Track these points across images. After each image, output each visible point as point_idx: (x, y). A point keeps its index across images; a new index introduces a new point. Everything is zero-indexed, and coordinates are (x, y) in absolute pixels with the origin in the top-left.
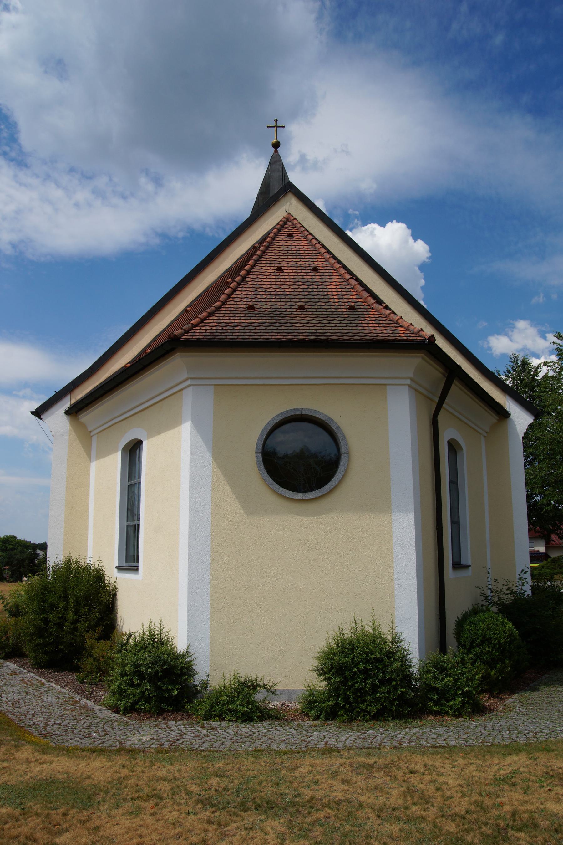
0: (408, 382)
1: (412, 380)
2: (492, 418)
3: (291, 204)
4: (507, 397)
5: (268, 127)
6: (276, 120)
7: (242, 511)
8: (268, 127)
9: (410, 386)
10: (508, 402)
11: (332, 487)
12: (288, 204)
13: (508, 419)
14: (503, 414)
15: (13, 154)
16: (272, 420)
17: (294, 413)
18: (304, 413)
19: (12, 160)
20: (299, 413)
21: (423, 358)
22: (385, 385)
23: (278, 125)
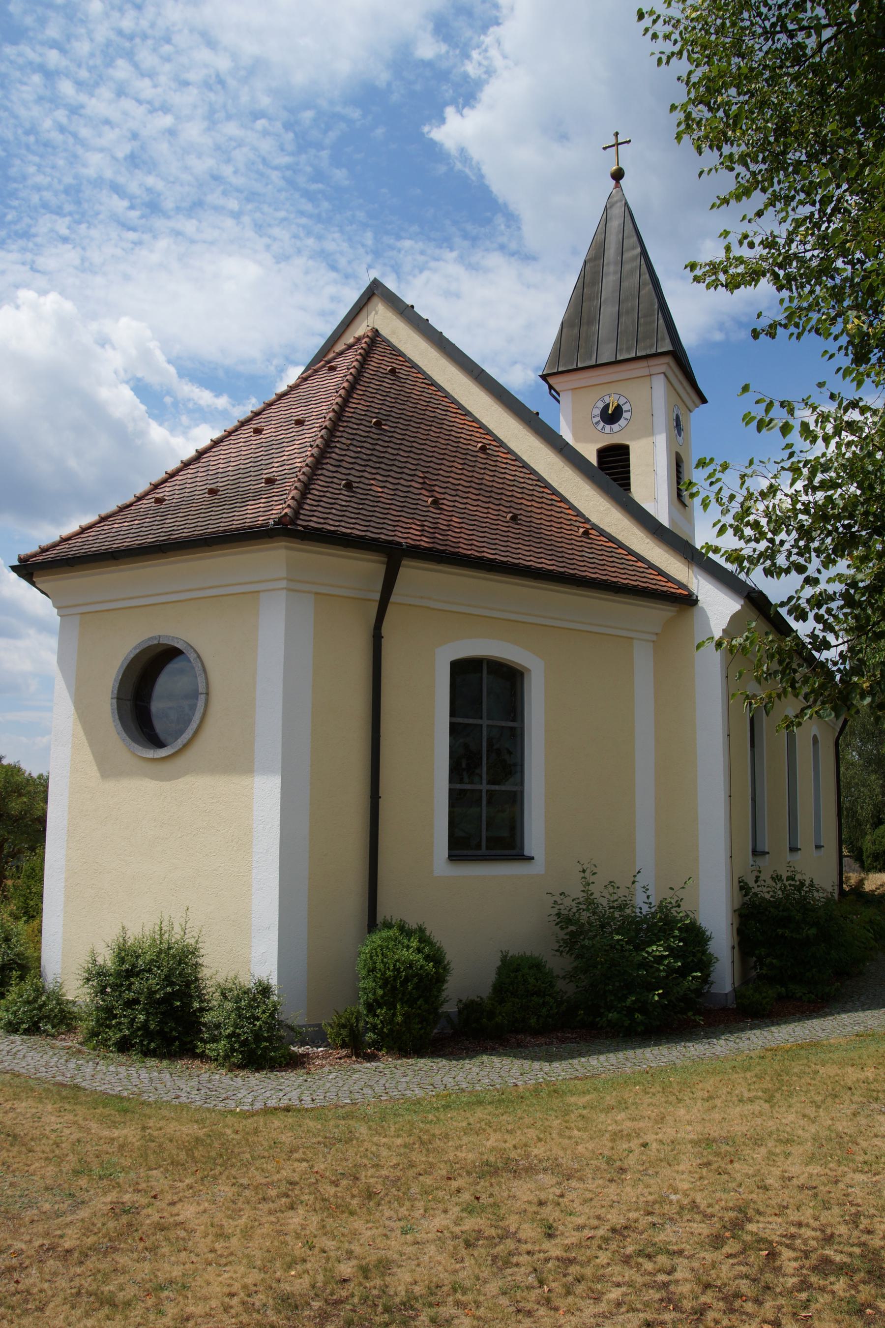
0: (284, 584)
1: (289, 580)
2: (659, 613)
3: (377, 313)
4: (696, 569)
5: (630, 141)
6: (617, 134)
7: (98, 775)
8: (605, 148)
9: (288, 589)
10: (697, 578)
11: (185, 741)
12: (374, 313)
13: (695, 609)
14: (688, 601)
15: (513, 246)
16: (129, 654)
17: (151, 643)
18: (162, 642)
19: (513, 254)
20: (156, 642)
21: (287, 548)
22: (258, 592)
23: (619, 141)
